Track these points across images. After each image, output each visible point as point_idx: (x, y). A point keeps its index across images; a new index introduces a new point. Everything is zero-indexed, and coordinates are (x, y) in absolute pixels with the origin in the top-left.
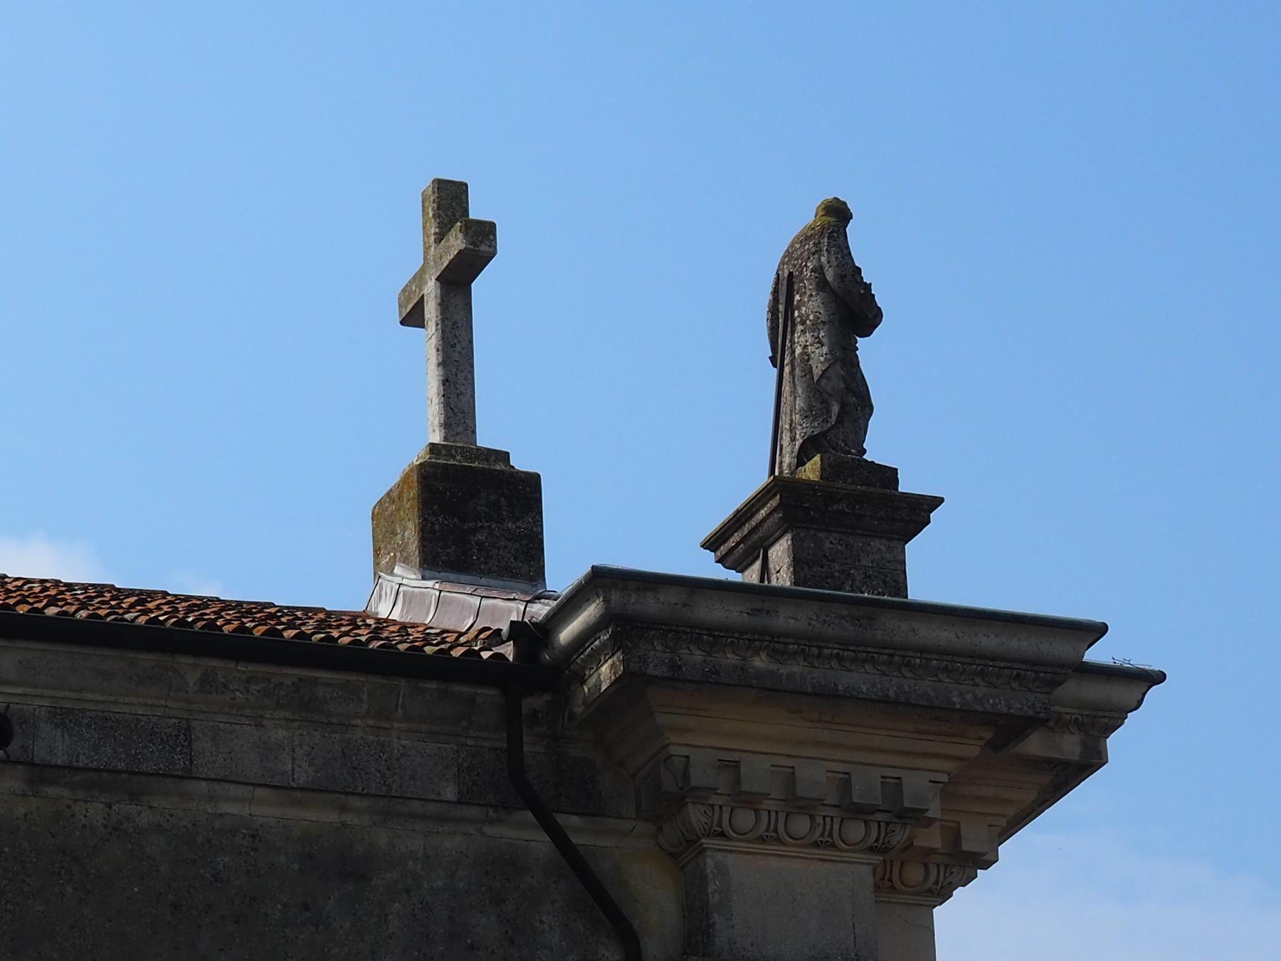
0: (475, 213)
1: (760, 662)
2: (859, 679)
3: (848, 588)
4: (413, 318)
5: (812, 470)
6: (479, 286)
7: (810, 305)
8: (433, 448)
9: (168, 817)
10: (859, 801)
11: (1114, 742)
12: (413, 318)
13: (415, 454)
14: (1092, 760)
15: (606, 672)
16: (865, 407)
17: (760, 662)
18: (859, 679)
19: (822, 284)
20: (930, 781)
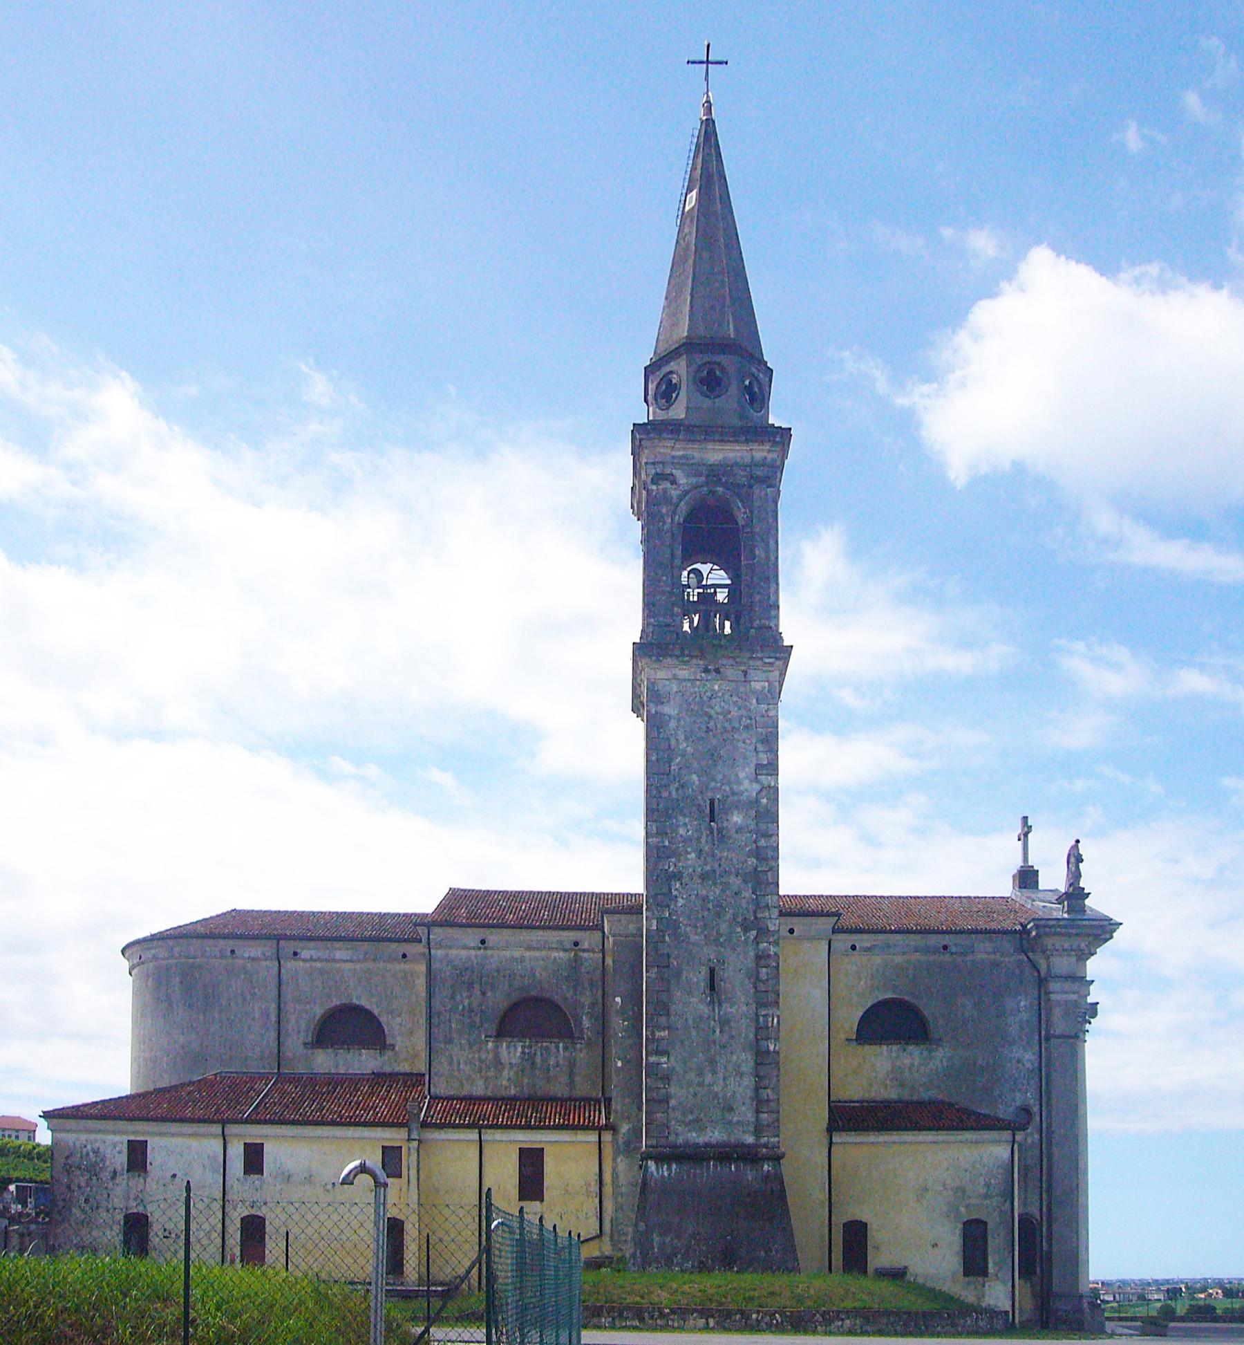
0: (1029, 824)
1: (1058, 930)
2: (1074, 931)
3: (649, 1143)
4: (1019, 840)
5: (1071, 889)
6: (1029, 835)
7: (1072, 860)
8: (1022, 867)
9: (111, 1211)
10: (895, 996)
11: (1114, 934)
12: (1019, 840)
13: (1018, 867)
14: (1111, 937)
15: (1034, 933)
16: (1081, 876)
17: (1058, 930)
18: (1074, 931)
19: (1074, 856)
20: (188, 1182)
